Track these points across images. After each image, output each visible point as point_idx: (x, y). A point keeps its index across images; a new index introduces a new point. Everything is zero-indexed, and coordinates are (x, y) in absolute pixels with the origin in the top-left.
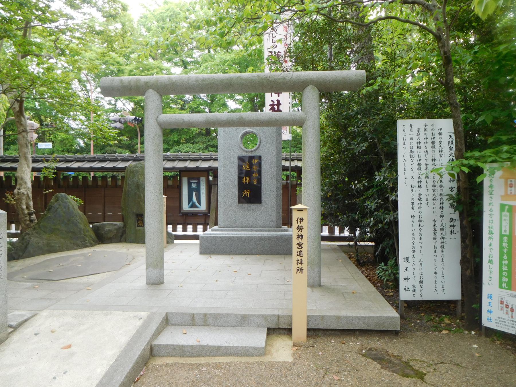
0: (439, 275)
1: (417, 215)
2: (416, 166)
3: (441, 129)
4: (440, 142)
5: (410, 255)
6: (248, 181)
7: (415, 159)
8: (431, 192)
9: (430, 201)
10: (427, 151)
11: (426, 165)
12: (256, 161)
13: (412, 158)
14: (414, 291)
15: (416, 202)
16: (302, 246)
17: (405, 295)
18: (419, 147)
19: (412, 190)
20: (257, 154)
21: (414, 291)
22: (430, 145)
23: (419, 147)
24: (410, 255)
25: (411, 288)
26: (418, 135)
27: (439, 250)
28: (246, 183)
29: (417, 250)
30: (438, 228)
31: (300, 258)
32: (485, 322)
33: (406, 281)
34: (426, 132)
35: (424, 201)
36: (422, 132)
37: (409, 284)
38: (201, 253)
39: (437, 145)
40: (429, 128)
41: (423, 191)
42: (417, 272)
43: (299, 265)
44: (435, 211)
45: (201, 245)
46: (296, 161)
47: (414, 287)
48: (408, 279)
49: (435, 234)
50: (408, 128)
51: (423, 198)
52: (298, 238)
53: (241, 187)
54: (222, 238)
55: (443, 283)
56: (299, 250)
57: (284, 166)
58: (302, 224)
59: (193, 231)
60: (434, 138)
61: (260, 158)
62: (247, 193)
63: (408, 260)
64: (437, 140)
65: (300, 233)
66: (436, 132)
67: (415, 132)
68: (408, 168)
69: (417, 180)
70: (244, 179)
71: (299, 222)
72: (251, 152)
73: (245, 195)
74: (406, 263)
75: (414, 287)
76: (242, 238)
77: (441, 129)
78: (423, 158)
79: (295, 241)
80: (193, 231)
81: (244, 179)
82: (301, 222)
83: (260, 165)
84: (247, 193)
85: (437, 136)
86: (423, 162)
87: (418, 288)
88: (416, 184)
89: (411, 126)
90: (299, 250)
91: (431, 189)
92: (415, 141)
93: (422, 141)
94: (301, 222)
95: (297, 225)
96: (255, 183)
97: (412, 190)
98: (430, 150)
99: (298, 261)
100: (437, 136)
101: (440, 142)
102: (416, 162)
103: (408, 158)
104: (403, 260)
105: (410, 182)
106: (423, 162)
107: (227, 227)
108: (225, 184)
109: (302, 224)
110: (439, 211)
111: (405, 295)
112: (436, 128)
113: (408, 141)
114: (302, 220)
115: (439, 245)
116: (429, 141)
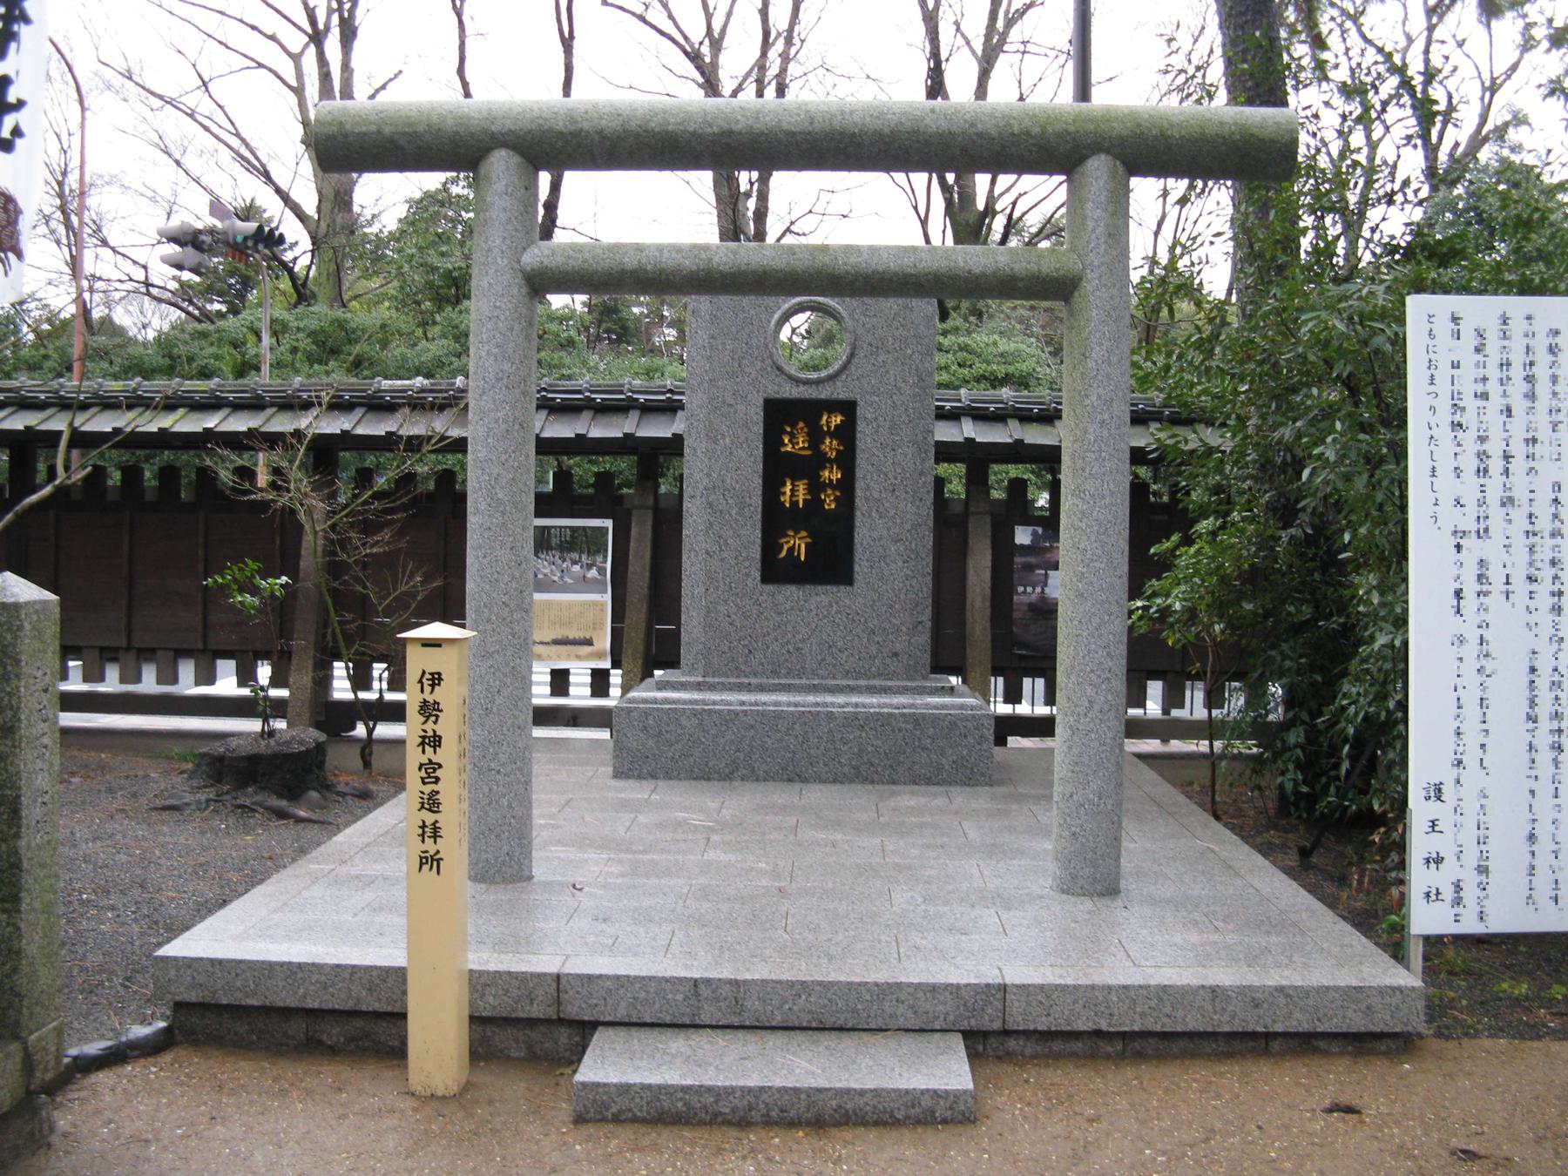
0: (1544, 846)
1: (1473, 636)
2: (1469, 463)
3: (1557, 333)
4: (1554, 379)
5: (1447, 776)
6: (802, 496)
7: (1468, 438)
8: (1520, 554)
9: (1520, 586)
10: (1509, 410)
11: (1507, 457)
12: (837, 419)
13: (1460, 434)
14: (1458, 901)
15: (1470, 588)
16: (439, 773)
17: (1426, 919)
18: (1485, 396)
19: (1458, 547)
20: (839, 392)
21: (1458, 901)
22: (1518, 387)
23: (1485, 396)
24: (1447, 776)
25: (1448, 893)
26: (1478, 350)
27: (1545, 756)
28: (794, 504)
29: (1470, 760)
30: (1543, 682)
31: (429, 818)
32: (960, 1035)
33: (1433, 866)
34: (1505, 343)
35: (1497, 585)
36: (1493, 345)
37: (1442, 879)
38: (618, 774)
39: (1543, 388)
40: (1517, 326)
41: (1490, 549)
42: (1469, 836)
43: (429, 841)
44: (1532, 619)
45: (619, 747)
46: (1013, 424)
47: (1458, 887)
48: (1439, 860)
49: (1532, 703)
50: (1443, 327)
51: (1496, 575)
52: (422, 744)
53: (775, 519)
54: (700, 715)
55: (1558, 875)
56: (428, 789)
57: (940, 445)
58: (439, 694)
59: (554, 693)
60: (1532, 364)
61: (848, 408)
62: (797, 543)
63: (1438, 792)
64: (1542, 372)
65: (429, 726)
66: (1541, 344)
67: (1469, 340)
68: (1445, 467)
69: (1472, 510)
70: (789, 487)
71: (427, 689)
72: (818, 382)
73: (791, 550)
74: (1434, 805)
75: (1458, 887)
76: (779, 715)
77: (1557, 333)
78: (1496, 436)
79: (414, 757)
80: (554, 693)
81: (789, 487)
82: (433, 686)
83: (847, 434)
84: (797, 543)
85: (1543, 358)
86: (1495, 448)
87: (1470, 893)
88: (1470, 525)
89: (1455, 319)
90: (428, 789)
91: (1520, 544)
92: (1468, 373)
93: (1493, 373)
94: (433, 686)
95: (420, 697)
96: (830, 504)
97: (1458, 547)
98: (1519, 405)
99: (423, 826)
100: (1543, 358)
101: (1554, 379)
102: (1471, 446)
103: (1444, 434)
104: (1424, 793)
105: (1452, 518)
106: (1495, 448)
107: (731, 668)
108: (710, 505)
109: (439, 694)
110: (1545, 619)
111: (1426, 919)
112: (1540, 327)
113: (1444, 372)
114: (436, 679)
115: (1544, 739)
116: (1517, 372)
